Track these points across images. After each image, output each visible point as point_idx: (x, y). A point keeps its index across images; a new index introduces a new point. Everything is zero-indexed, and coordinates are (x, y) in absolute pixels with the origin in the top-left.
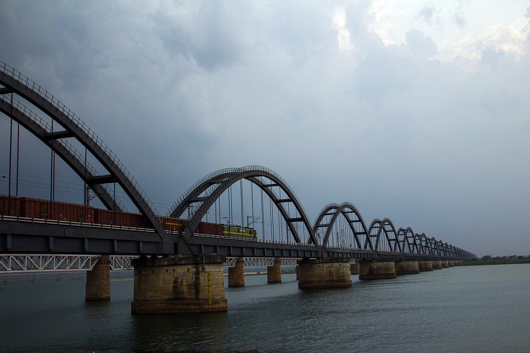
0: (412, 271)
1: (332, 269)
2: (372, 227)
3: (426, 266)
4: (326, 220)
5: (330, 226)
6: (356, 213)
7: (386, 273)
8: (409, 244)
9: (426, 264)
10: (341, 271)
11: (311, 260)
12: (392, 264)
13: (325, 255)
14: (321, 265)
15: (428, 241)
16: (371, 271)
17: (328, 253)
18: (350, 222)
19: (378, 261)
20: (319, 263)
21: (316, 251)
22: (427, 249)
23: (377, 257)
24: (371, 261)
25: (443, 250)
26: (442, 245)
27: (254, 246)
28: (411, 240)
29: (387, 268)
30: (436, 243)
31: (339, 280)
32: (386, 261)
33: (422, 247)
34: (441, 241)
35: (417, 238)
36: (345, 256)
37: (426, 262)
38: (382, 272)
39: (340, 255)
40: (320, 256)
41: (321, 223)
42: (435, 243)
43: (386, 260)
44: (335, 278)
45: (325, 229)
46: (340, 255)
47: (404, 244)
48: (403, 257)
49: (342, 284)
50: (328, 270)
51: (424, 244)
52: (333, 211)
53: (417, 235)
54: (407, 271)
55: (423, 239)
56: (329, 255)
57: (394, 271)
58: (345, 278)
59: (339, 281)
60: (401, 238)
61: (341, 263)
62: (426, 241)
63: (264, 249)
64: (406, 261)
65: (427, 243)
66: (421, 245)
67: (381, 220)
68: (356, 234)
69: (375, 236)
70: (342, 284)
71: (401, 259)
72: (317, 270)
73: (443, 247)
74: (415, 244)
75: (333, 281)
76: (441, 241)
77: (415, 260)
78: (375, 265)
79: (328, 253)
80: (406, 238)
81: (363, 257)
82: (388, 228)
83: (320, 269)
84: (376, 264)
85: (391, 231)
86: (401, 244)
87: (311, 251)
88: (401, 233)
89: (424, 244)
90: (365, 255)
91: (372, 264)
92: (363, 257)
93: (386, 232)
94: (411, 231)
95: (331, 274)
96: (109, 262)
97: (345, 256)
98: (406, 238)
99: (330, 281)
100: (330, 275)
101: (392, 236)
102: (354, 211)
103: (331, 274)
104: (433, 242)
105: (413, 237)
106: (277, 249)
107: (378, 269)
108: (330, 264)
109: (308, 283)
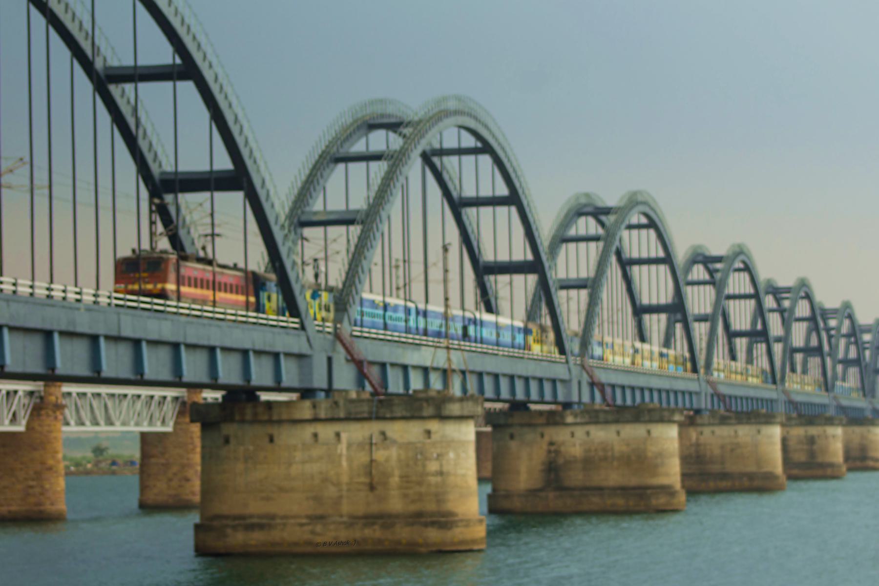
0: (751, 476)
1: (380, 455)
2: (561, 239)
3: (812, 454)
4: (347, 189)
5: (365, 221)
6: (498, 162)
7: (634, 481)
8: (732, 335)
9: (811, 440)
10: (433, 466)
11: (269, 405)
12: (671, 432)
13: (345, 378)
14: (326, 431)
15: (769, 302)
16: (553, 469)
17: (359, 364)
18: (458, 206)
19: (593, 417)
20: (316, 420)
21: (300, 357)
22: (817, 360)
23: (586, 398)
24: (553, 419)
25: (857, 362)
26: (855, 333)
27: (56, 320)
28: (741, 315)
29: (640, 459)
30: (817, 318)
31: (419, 515)
32: (414, 416)
33: (732, 335)
34: (847, 306)
35: (769, 302)
36: (456, 389)
37: (813, 431)
38: (613, 478)
39: (436, 383)
40: (319, 381)
41: (317, 205)
42: (812, 319)
43: (638, 414)
44: (396, 504)
45: (341, 239)
46: (436, 383)
47: (593, 302)
48: (704, 403)
49: (433, 535)
50: (363, 458)
51: (799, 334)
52: (378, 141)
53: (776, 292)
54: (724, 476)
55: (738, 283)
56: (362, 377)
57: (672, 473)
58: (450, 506)
59: (418, 518)
60: (700, 300)
61: (434, 426)
62: (756, 296)
63: (48, 335)
64: (724, 421)
65: (760, 312)
66: (719, 315)
67: (611, 198)
68: (484, 270)
69: (580, 285)
70: (433, 535)
71: (698, 412)
72: (299, 455)
73: (861, 347)
74: (758, 334)
75: (385, 519)
76: (847, 306)
77: (660, 417)
78: (576, 439)
79: (359, 364)
80: (722, 297)
81: (505, 394)
82: (639, 244)
83: (316, 452)
84: (580, 432)
85: (656, 261)
86: (700, 330)
87: (276, 356)
88: (699, 272)
89: (741, 315)
90: (519, 385)
91: (560, 435)
92: (505, 394)
93: (626, 264)
94: (747, 268)
95: (373, 480)
96: (59, 407)
97: (456, 389)
98: (722, 297)
99: (370, 519)
100: (372, 487)
101: (654, 286)
102: (486, 148)
103: (373, 480)
104: (803, 309)
105: (756, 296)
106: (67, 334)
107: (589, 462)
108: (373, 428)
109: (251, 527)
